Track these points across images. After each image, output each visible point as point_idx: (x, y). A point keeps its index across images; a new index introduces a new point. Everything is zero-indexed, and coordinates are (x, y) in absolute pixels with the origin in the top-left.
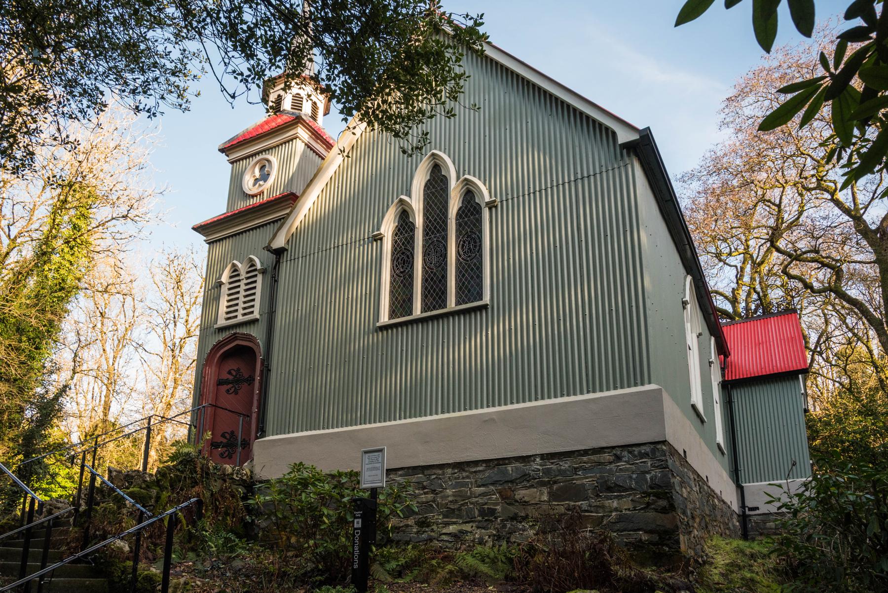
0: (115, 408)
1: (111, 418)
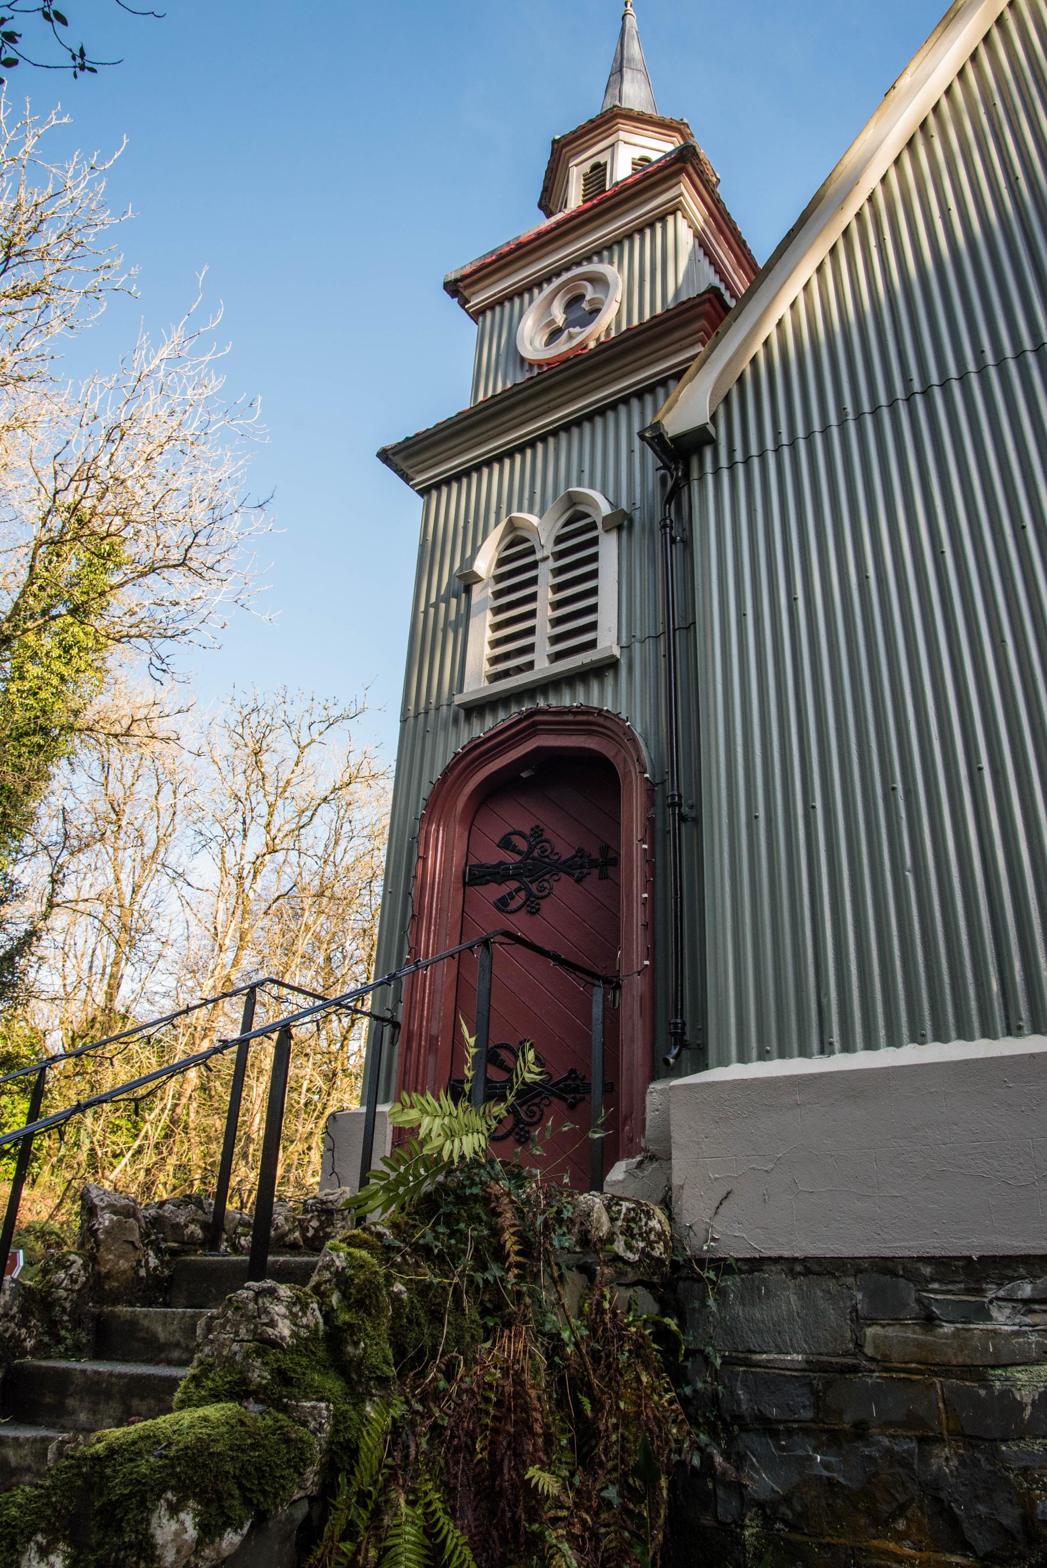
0: (126, 990)
1: (119, 1006)
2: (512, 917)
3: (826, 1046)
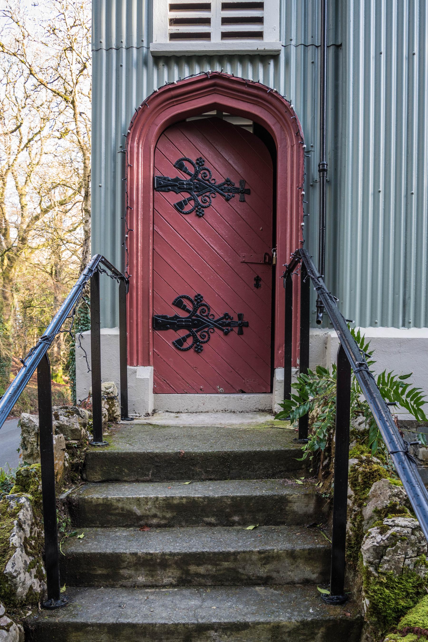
2: (186, 217)
3: (406, 324)
